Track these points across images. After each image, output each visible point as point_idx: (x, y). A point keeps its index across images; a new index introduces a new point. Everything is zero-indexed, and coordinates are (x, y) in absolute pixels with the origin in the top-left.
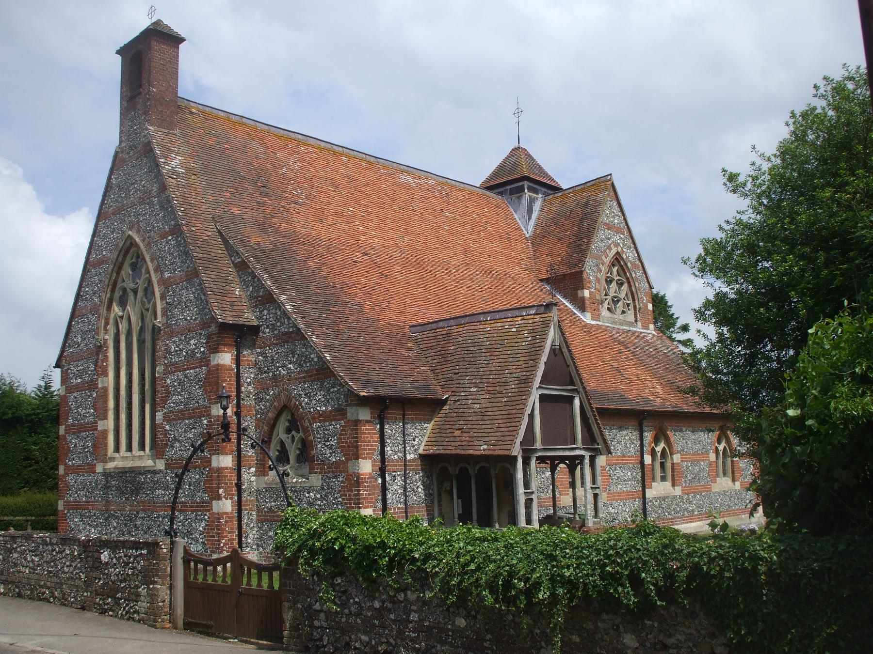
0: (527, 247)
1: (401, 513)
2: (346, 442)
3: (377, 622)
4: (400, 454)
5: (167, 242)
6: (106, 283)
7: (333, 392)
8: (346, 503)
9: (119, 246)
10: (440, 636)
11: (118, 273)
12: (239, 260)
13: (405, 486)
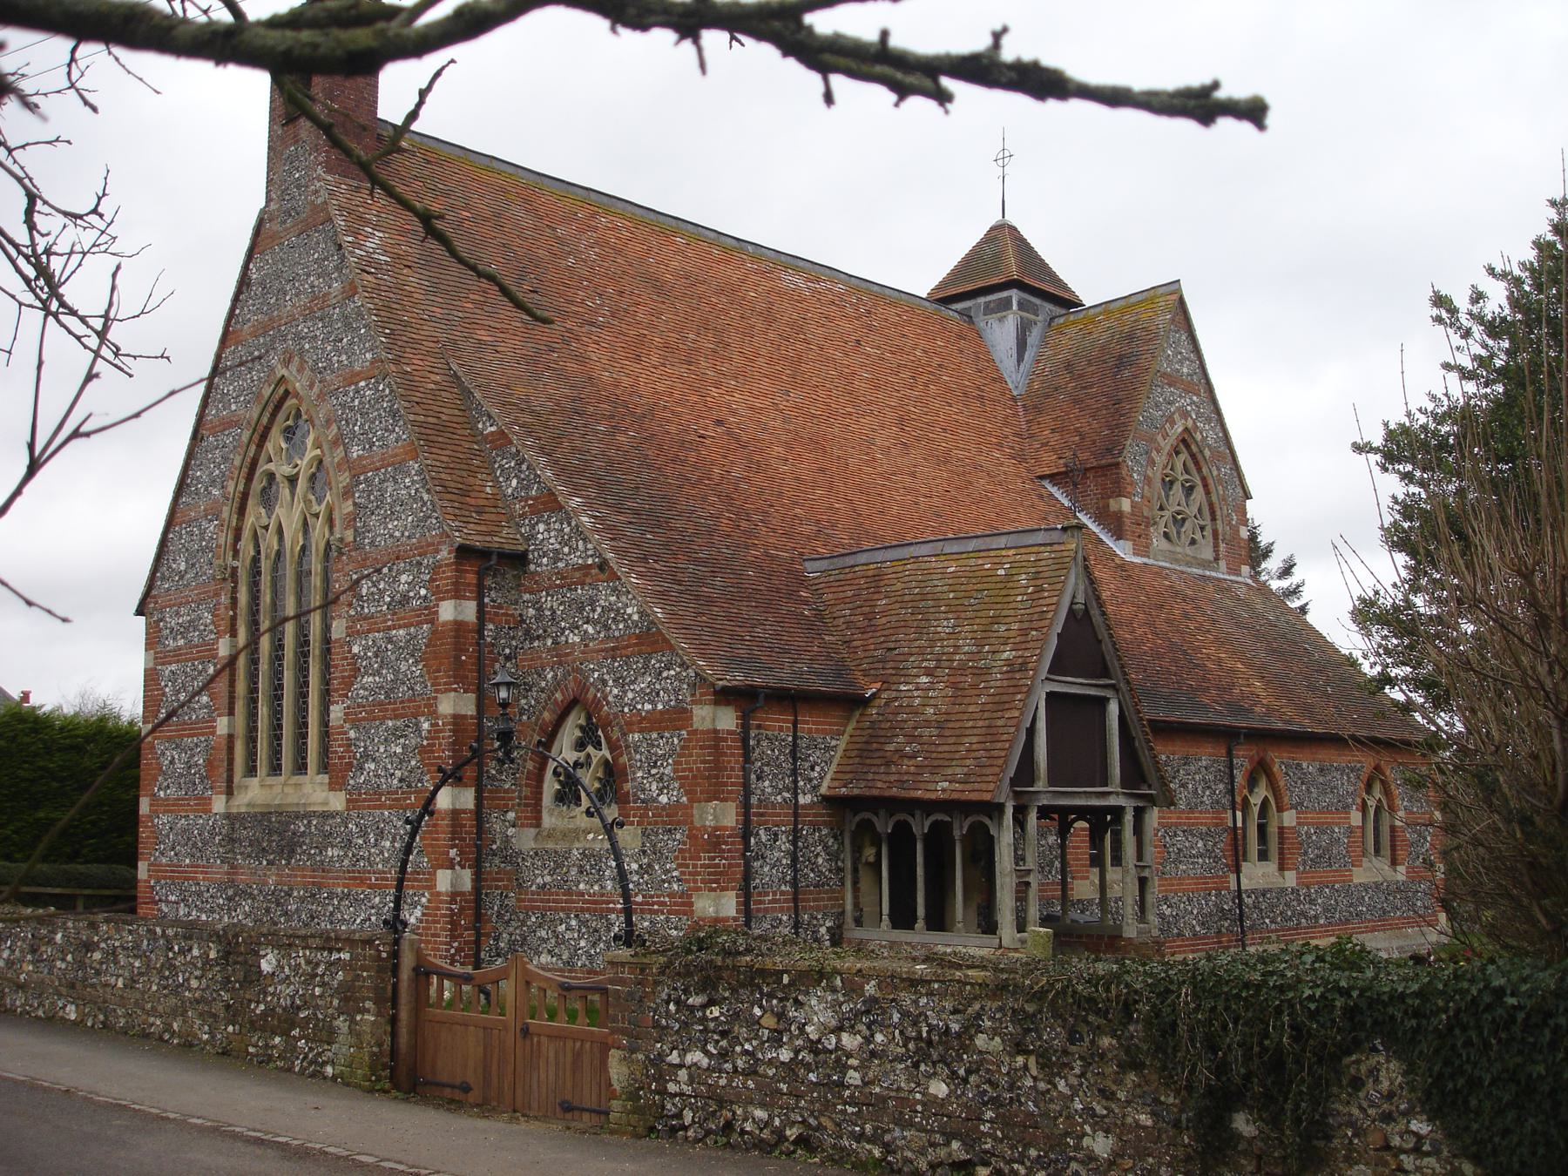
0: (1016, 415)
1: (786, 901)
2: (691, 770)
3: (784, 1087)
4: (786, 795)
5: (357, 392)
6: (237, 462)
7: (667, 678)
8: (687, 881)
9: (263, 396)
10: (901, 1113)
11: (260, 446)
12: (493, 429)
13: (795, 852)
